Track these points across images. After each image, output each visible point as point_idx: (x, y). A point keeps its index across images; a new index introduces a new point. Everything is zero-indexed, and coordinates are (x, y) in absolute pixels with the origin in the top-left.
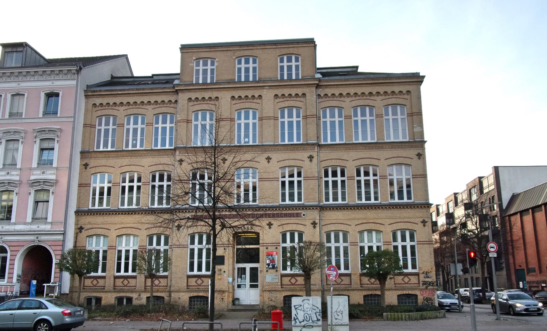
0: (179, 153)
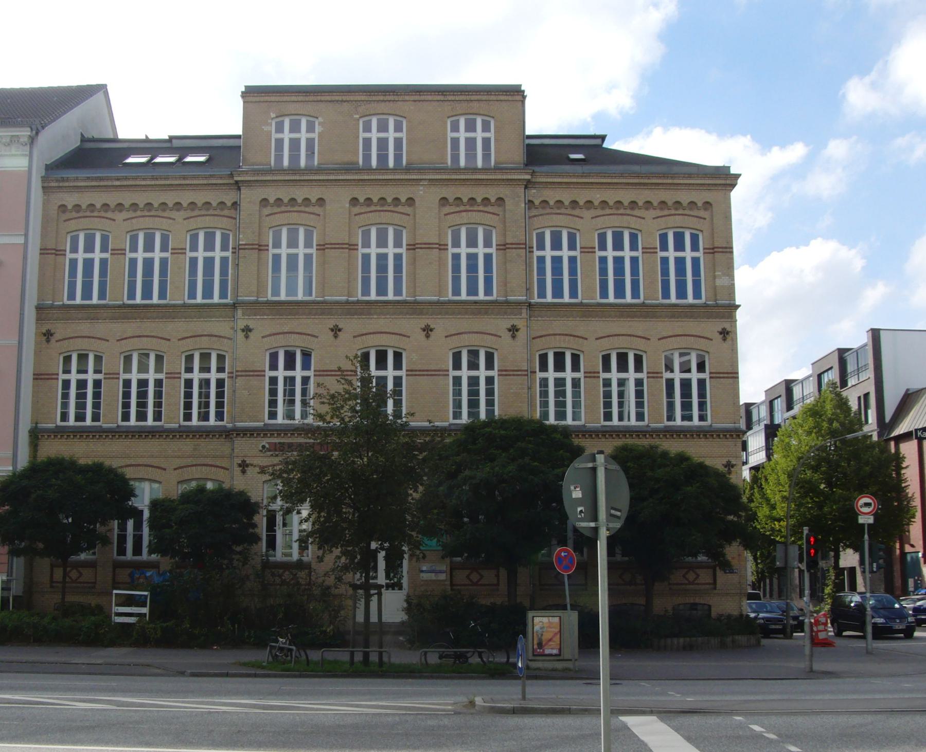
0: (243, 314)
